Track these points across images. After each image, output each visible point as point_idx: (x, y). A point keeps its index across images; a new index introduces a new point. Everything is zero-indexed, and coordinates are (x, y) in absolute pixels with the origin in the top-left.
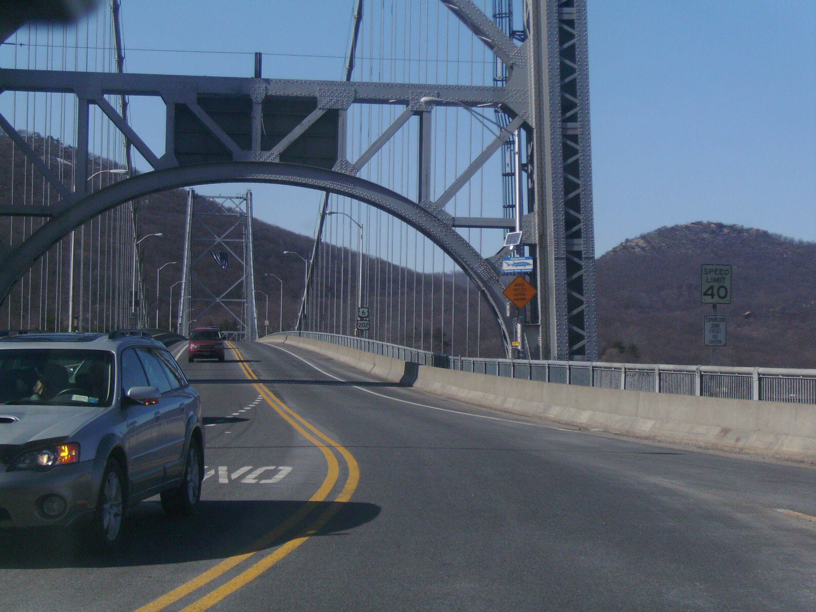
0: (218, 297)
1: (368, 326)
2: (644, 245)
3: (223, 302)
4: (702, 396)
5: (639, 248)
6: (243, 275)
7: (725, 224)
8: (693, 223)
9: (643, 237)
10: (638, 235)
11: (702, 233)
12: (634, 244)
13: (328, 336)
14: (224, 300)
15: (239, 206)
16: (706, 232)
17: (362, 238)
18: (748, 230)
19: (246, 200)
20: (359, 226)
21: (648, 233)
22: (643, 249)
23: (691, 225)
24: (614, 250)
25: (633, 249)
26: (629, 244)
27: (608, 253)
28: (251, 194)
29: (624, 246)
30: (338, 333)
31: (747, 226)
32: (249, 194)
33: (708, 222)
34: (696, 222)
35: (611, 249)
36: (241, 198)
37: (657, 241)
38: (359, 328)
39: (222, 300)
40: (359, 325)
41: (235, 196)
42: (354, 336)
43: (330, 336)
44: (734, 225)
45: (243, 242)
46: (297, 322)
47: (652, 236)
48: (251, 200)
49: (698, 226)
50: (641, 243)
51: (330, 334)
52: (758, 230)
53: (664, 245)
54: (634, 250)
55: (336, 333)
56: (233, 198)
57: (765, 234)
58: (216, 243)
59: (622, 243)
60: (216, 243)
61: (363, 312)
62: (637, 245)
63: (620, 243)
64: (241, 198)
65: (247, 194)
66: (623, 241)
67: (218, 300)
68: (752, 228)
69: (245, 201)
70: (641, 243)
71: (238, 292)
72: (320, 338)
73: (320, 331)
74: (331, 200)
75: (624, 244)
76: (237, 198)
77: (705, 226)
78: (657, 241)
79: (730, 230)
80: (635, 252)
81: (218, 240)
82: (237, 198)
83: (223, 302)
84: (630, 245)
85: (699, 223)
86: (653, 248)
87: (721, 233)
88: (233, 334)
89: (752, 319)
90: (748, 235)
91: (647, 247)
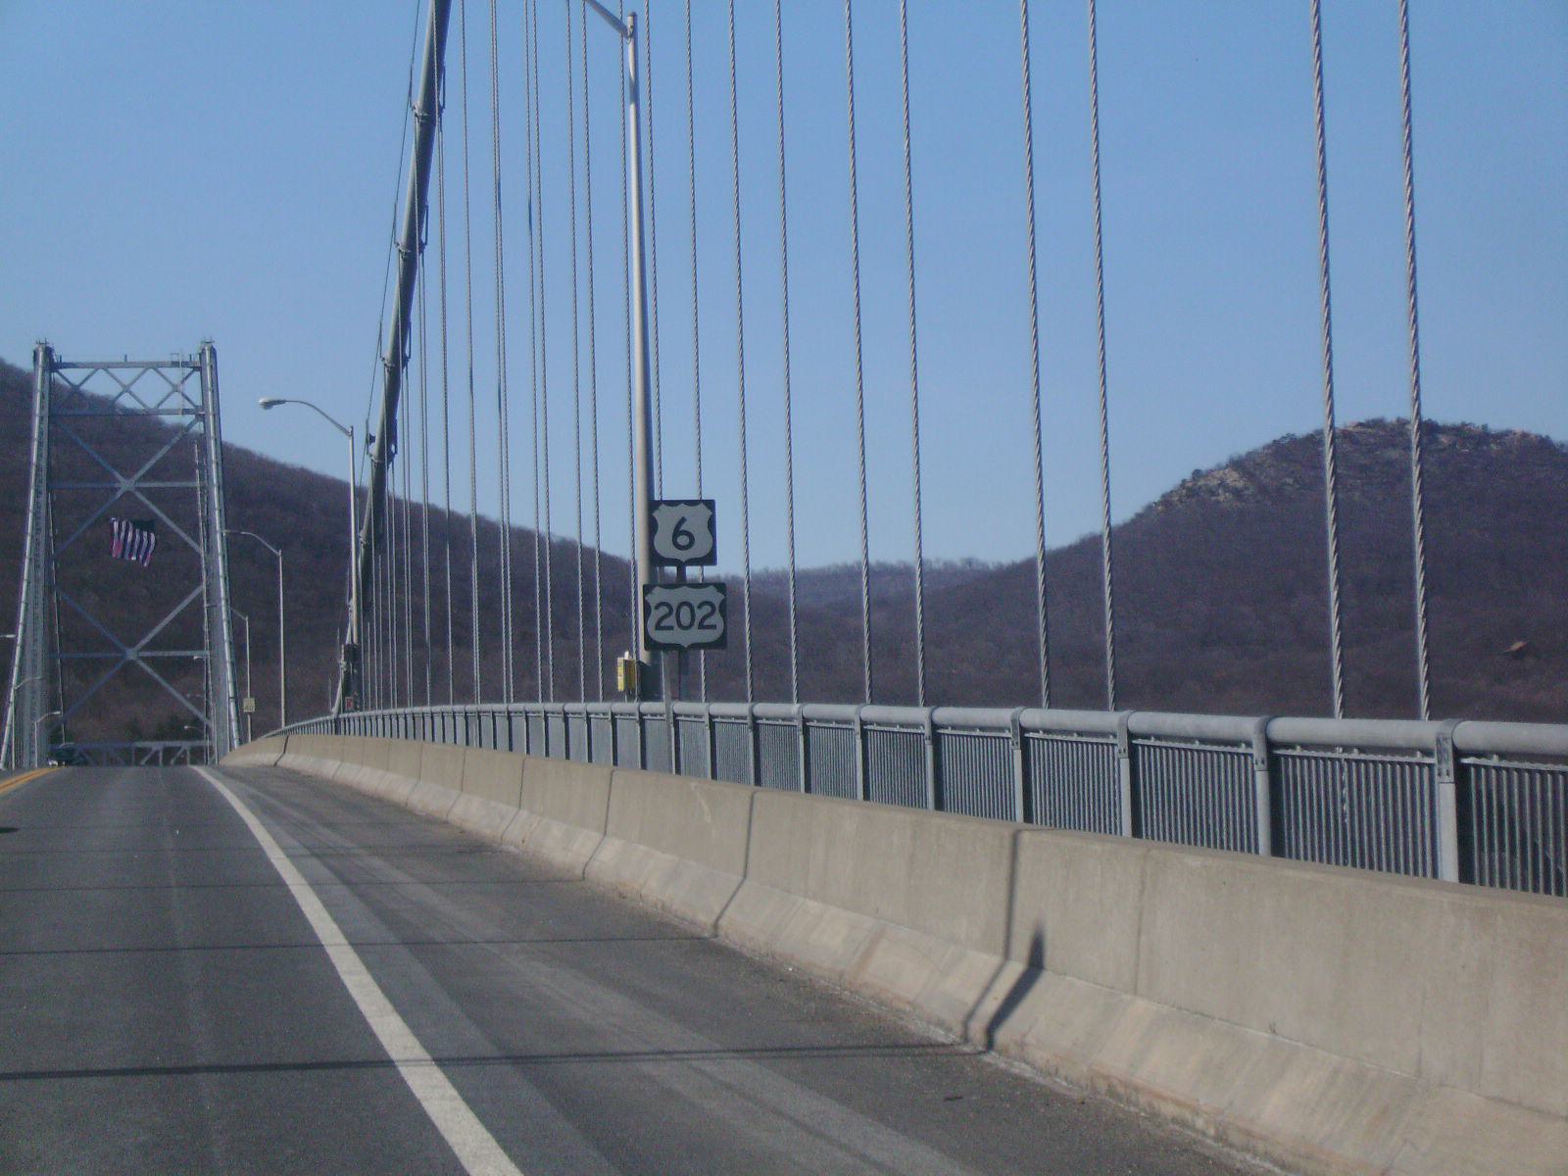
0: (132, 645)
1: (716, 619)
2: (1240, 484)
3: (144, 659)
4: (1141, 837)
5: (1229, 491)
6: (199, 580)
7: (1440, 423)
8: (1360, 424)
9: (1236, 464)
10: (1224, 459)
11: (1385, 448)
12: (1216, 482)
13: (449, 721)
14: (147, 654)
15: (181, 388)
16: (1394, 446)
17: (635, 98)
18: (1500, 437)
19: (199, 369)
20: (618, 24)
21: (1249, 454)
22: (1237, 493)
23: (1356, 430)
24: (1166, 500)
25: (1213, 493)
26: (1201, 483)
27: (1150, 508)
28: (213, 352)
29: (1188, 489)
30: (493, 694)
31: (1496, 425)
32: (207, 353)
33: (1398, 420)
34: (1368, 422)
35: (1157, 498)
36: (185, 364)
37: (1272, 472)
38: (660, 637)
39: (141, 654)
40: (655, 615)
41: (169, 359)
42: (611, 694)
43: (460, 720)
44: (1464, 425)
45: (194, 489)
46: (335, 687)
47: (1258, 461)
48: (214, 368)
49: (1374, 431)
50: (1233, 479)
51: (458, 708)
52: (1525, 435)
53: (1290, 481)
54: (1213, 498)
55: (486, 699)
56: (163, 365)
57: (1544, 444)
58: (119, 494)
59: (1184, 481)
60: (119, 494)
61: (677, 532)
62: (1222, 484)
63: (1178, 482)
64: (185, 364)
65: (202, 354)
66: (1187, 475)
67: (131, 654)
68: (1511, 431)
69: (197, 374)
70: (1233, 479)
71: (190, 630)
72: (414, 729)
73: (420, 700)
74: (441, 194)
75: (1190, 484)
76: (175, 364)
77: (1392, 430)
78: (1272, 472)
79: (1455, 438)
80: (1218, 502)
81: (125, 484)
82: (175, 364)
83: (144, 659)
84: (1206, 485)
85: (1377, 424)
86: (1262, 489)
87: (1433, 447)
88: (180, 748)
89: (1530, 661)
90: (1499, 448)
91: (1246, 488)
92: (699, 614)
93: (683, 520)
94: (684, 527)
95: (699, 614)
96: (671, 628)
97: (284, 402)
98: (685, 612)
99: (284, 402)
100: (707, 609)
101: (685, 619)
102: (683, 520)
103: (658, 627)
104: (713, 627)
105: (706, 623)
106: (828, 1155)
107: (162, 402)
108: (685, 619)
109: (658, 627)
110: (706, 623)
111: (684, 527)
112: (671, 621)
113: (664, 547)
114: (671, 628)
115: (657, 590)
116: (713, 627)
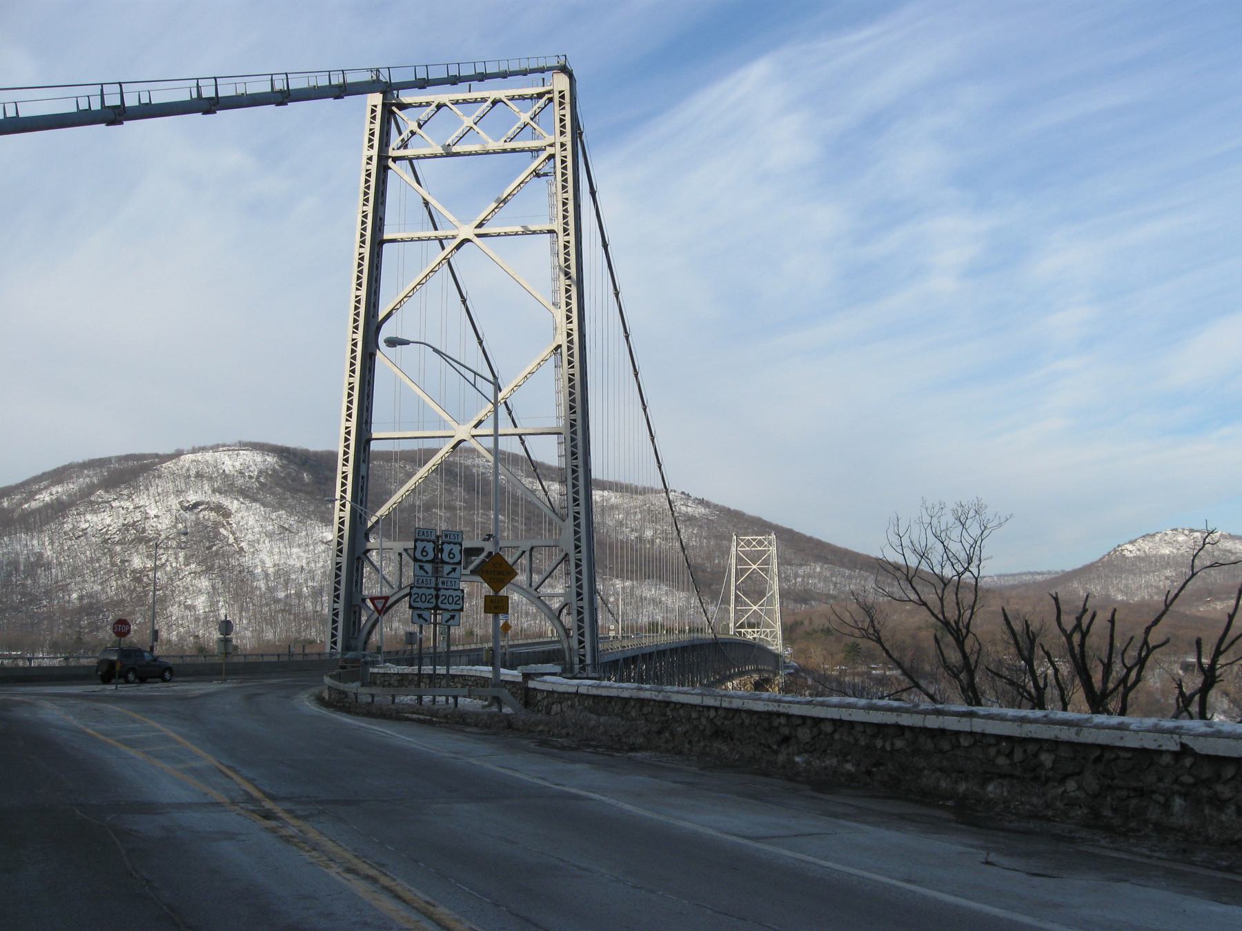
1: (434, 600)
21: (734, 510)
61: (450, 553)
92: (455, 599)
93: (425, 547)
94: (425, 549)
95: (455, 599)
96: (418, 602)
97: (406, 343)
98: (451, 599)
99: (406, 343)
100: (431, 596)
101: (451, 601)
102: (425, 547)
103: (414, 601)
104: (459, 604)
105: (430, 601)
106: (995, 644)
107: (471, 383)
108: (451, 601)
109: (414, 601)
110: (430, 601)
111: (425, 549)
112: (419, 599)
113: (419, 556)
114: (418, 602)
115: (415, 589)
116: (459, 604)
